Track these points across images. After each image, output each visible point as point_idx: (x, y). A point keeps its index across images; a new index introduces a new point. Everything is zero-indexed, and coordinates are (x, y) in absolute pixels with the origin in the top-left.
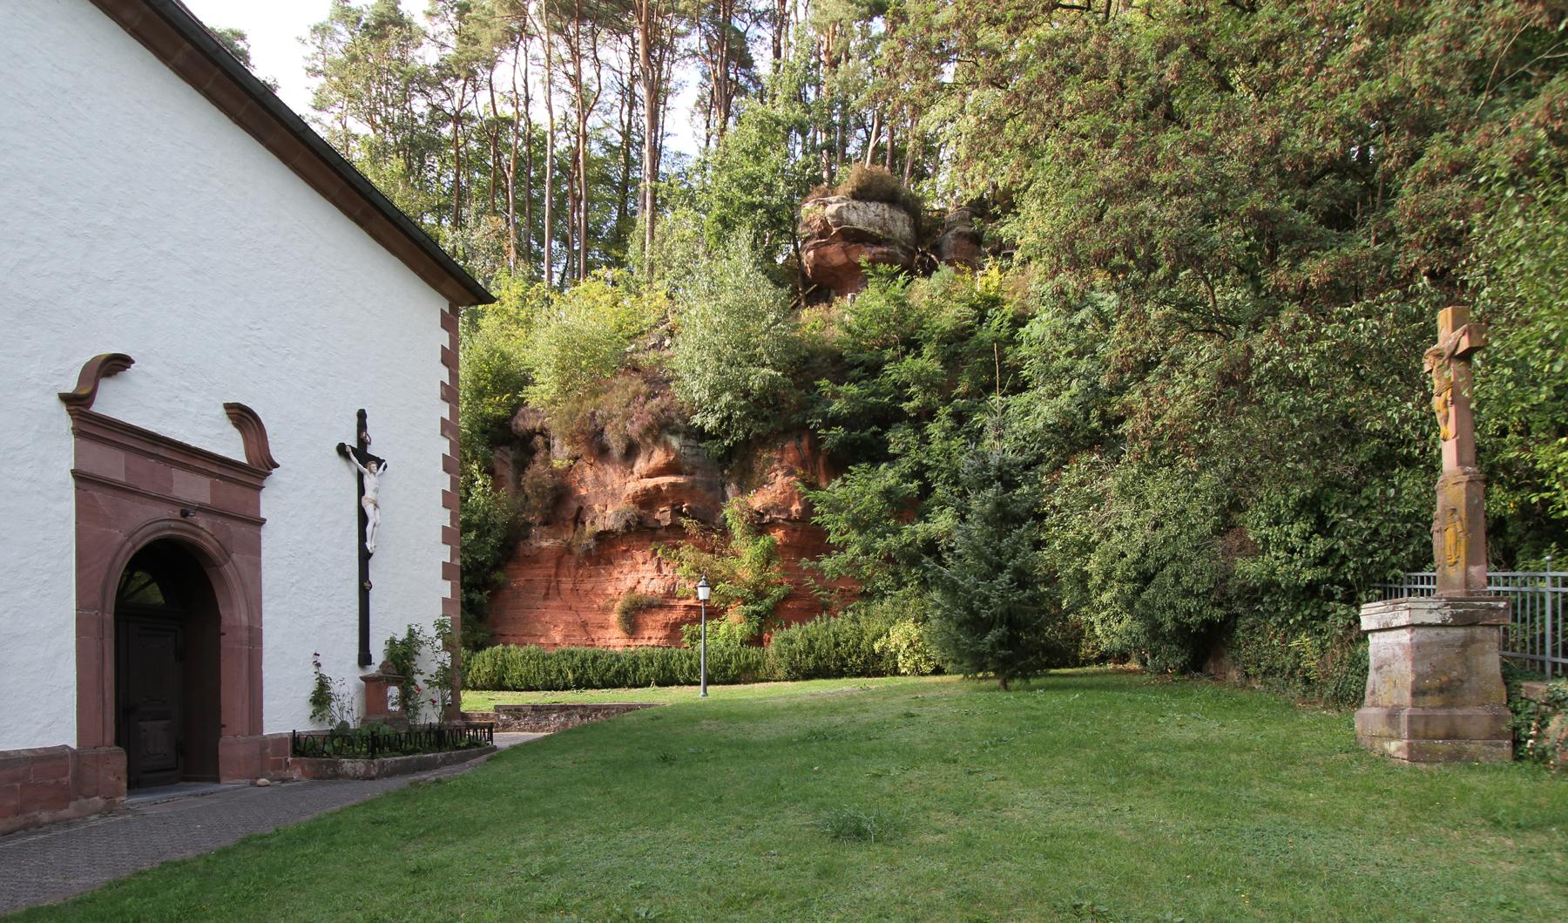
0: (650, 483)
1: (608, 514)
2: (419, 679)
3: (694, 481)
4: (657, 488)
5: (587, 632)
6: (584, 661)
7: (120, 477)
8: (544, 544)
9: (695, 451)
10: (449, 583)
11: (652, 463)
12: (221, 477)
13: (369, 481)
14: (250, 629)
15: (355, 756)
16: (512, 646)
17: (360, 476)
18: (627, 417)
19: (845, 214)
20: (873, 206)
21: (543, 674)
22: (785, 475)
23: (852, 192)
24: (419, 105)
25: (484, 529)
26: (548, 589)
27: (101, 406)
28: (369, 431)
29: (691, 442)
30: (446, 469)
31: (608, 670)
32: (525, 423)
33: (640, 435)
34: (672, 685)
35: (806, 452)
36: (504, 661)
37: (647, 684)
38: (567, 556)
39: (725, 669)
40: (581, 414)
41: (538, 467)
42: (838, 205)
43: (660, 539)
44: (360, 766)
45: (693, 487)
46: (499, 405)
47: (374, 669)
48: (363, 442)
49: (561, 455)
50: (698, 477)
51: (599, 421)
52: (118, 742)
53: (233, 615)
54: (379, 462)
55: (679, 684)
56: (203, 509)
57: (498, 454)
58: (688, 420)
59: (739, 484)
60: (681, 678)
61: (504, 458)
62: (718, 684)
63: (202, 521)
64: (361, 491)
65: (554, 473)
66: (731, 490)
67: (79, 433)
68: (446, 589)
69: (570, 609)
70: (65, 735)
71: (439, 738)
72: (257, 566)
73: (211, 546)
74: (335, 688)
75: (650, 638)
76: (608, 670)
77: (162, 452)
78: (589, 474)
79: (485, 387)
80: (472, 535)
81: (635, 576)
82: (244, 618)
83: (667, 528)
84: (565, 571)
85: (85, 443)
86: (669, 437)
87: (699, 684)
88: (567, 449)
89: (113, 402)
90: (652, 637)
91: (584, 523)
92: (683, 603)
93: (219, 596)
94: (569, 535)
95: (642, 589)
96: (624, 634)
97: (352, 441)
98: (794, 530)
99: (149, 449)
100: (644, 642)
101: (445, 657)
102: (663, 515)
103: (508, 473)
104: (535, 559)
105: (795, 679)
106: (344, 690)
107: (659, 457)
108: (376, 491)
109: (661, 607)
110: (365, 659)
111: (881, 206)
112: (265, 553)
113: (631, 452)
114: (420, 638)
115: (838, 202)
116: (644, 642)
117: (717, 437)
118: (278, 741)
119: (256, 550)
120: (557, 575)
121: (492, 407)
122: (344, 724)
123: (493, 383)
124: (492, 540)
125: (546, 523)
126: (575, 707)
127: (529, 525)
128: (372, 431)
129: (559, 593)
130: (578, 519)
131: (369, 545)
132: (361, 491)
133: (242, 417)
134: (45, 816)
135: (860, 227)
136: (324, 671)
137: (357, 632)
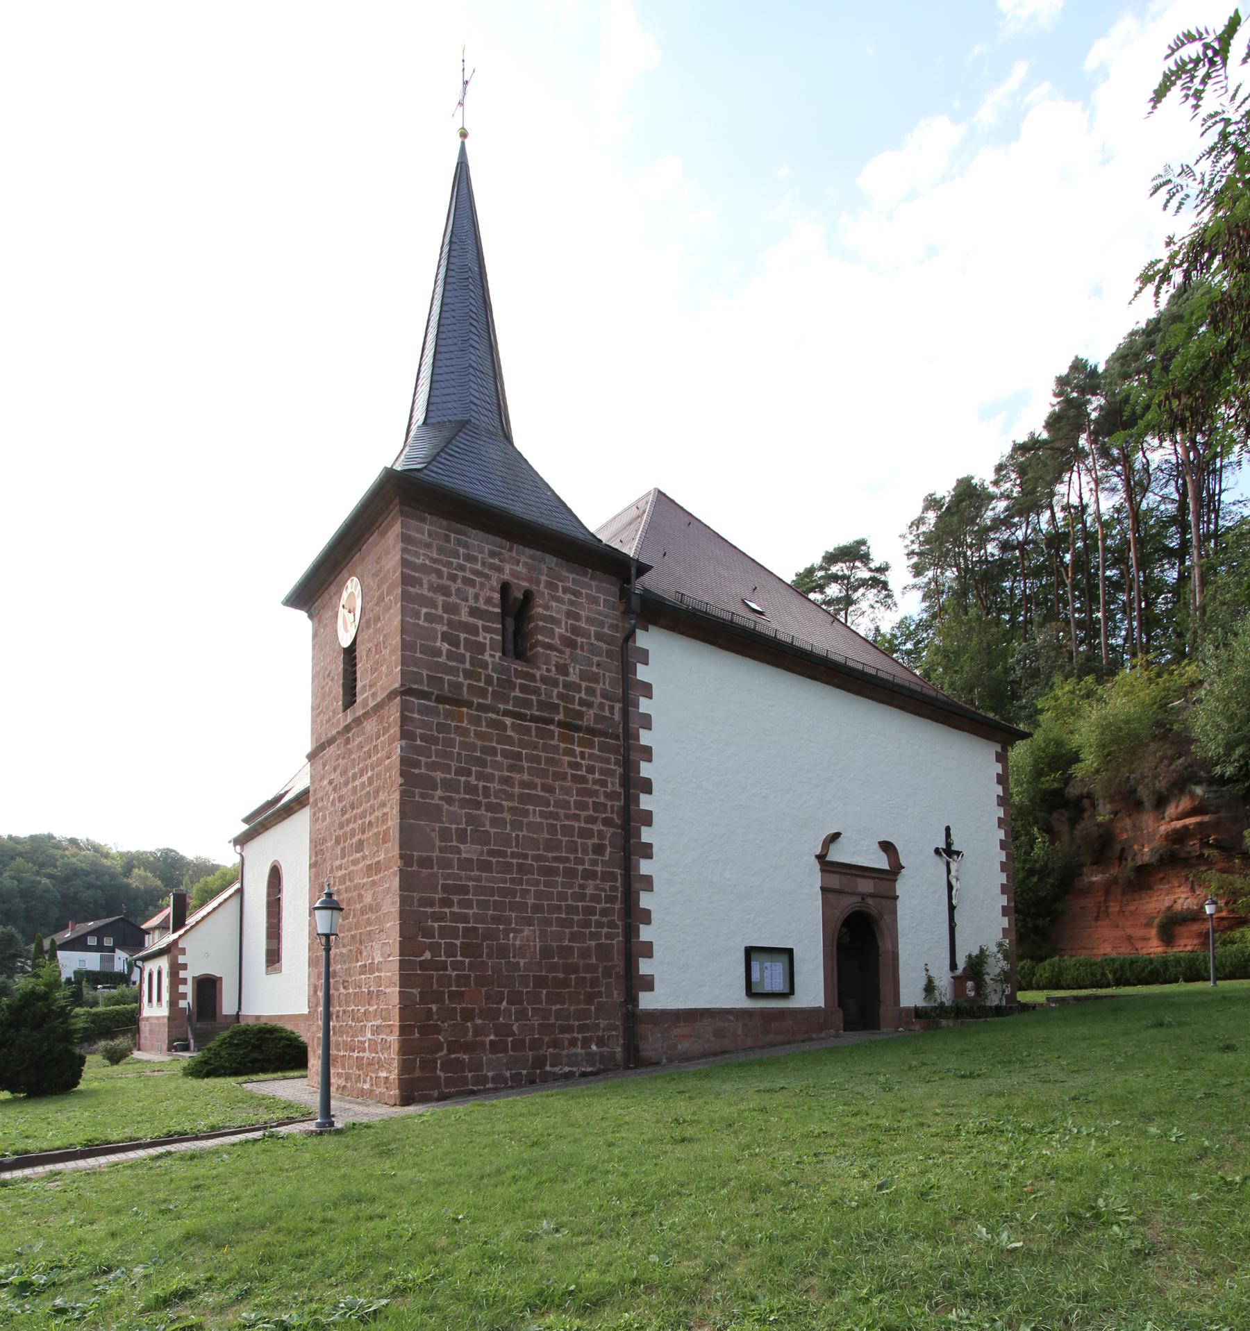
0: (1179, 824)
1: (1146, 853)
2: (987, 978)
4: (1185, 827)
5: (1132, 944)
6: (1122, 966)
7: (837, 886)
8: (1094, 879)
9: (1219, 794)
10: (1007, 919)
11: (1180, 808)
12: (878, 878)
13: (953, 866)
14: (893, 952)
15: (948, 1018)
16: (1066, 957)
17: (948, 864)
18: (1156, 777)
21: (1090, 976)
24: (992, 548)
25: (1043, 872)
26: (1099, 912)
27: (829, 858)
28: (952, 837)
29: (1214, 788)
30: (1002, 848)
31: (1143, 971)
32: (1073, 791)
33: (1168, 790)
36: (1060, 968)
40: (1118, 779)
41: (1085, 825)
43: (1192, 866)
44: (951, 1023)
46: (1054, 780)
47: (959, 971)
48: (949, 844)
49: (1103, 814)
50: (1223, 814)
51: (1133, 782)
52: (840, 1005)
53: (886, 945)
54: (958, 853)
56: (871, 895)
57: (1055, 815)
58: (1210, 772)
61: (1060, 819)
62: (1239, 978)
63: (870, 901)
64: (949, 872)
65: (1099, 825)
67: (822, 870)
68: (1005, 922)
69: (1117, 926)
70: (820, 1002)
71: (998, 1011)
72: (895, 920)
73: (874, 912)
74: (936, 983)
75: (1185, 946)
76: (1143, 971)
77: (853, 872)
78: (1128, 823)
79: (1043, 769)
80: (1035, 879)
81: (1173, 897)
82: (890, 947)
85: (828, 875)
86: (1193, 787)
88: (1108, 806)
89: (836, 855)
90: (1186, 945)
91: (1126, 859)
93: (878, 939)
94: (1115, 871)
95: (1178, 907)
97: (942, 845)
99: (848, 871)
100: (1180, 949)
101: (1003, 963)
102: (1193, 845)
103: (1064, 828)
104: (1088, 891)
106: (942, 983)
107: (1185, 803)
108: (957, 871)
110: (953, 966)
112: (899, 913)
113: (1161, 802)
114: (987, 953)
117: (1237, 781)
118: (907, 1010)
119: (895, 912)
120: (1106, 901)
121: (1050, 781)
122: (942, 1003)
123: (1049, 765)
124: (1051, 881)
125: (1095, 863)
127: (1081, 866)
128: (1156, 81)
129: (1108, 915)
130: (1121, 857)
132: (949, 872)
133: (887, 847)
134: (814, 1036)
136: (930, 973)
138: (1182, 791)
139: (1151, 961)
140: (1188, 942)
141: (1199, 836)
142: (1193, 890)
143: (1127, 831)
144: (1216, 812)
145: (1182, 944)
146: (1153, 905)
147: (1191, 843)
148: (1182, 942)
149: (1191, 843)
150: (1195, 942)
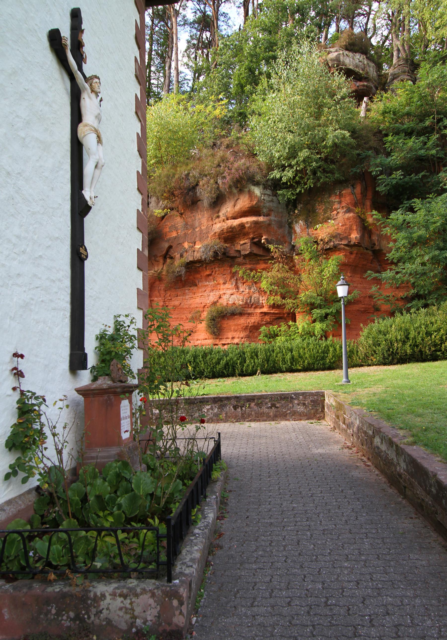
3: (270, 220)
4: (242, 226)
6: (195, 357)
11: (238, 208)
19: (341, 58)
20: (358, 56)
22: (345, 212)
23: (346, 46)
31: (218, 363)
34: (276, 372)
35: (359, 196)
37: (253, 373)
38: (157, 283)
39: (323, 358)
40: (177, 176)
42: (336, 53)
45: (269, 225)
50: (272, 218)
55: (282, 372)
59: (306, 221)
60: (284, 367)
62: (317, 370)
66: (299, 227)
75: (233, 338)
76: (218, 363)
78: (179, 221)
81: (217, 293)
83: (245, 256)
84: (156, 293)
86: (252, 187)
87: (341, 368)
92: (259, 311)
95: (224, 301)
96: (211, 336)
98: (351, 253)
105: (391, 363)
109: (241, 314)
111: (362, 56)
115: (336, 51)
116: (229, 341)
117: (291, 186)
126: (228, 398)
131: (87, 194)
135: (351, 67)
137: (67, 321)
138: (241, 191)
139: (226, 354)
140: (236, 334)
141: (251, 236)
142: (237, 288)
143: (177, 230)
144: (268, 215)
145: (230, 337)
146: (198, 300)
147: (242, 242)
148: (230, 335)
149: (242, 242)
150: (242, 335)
